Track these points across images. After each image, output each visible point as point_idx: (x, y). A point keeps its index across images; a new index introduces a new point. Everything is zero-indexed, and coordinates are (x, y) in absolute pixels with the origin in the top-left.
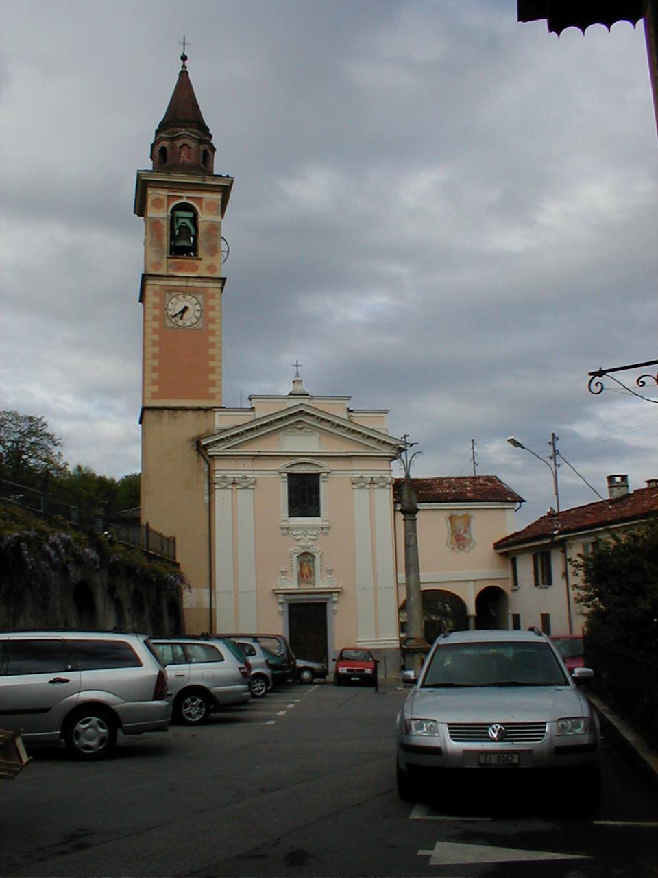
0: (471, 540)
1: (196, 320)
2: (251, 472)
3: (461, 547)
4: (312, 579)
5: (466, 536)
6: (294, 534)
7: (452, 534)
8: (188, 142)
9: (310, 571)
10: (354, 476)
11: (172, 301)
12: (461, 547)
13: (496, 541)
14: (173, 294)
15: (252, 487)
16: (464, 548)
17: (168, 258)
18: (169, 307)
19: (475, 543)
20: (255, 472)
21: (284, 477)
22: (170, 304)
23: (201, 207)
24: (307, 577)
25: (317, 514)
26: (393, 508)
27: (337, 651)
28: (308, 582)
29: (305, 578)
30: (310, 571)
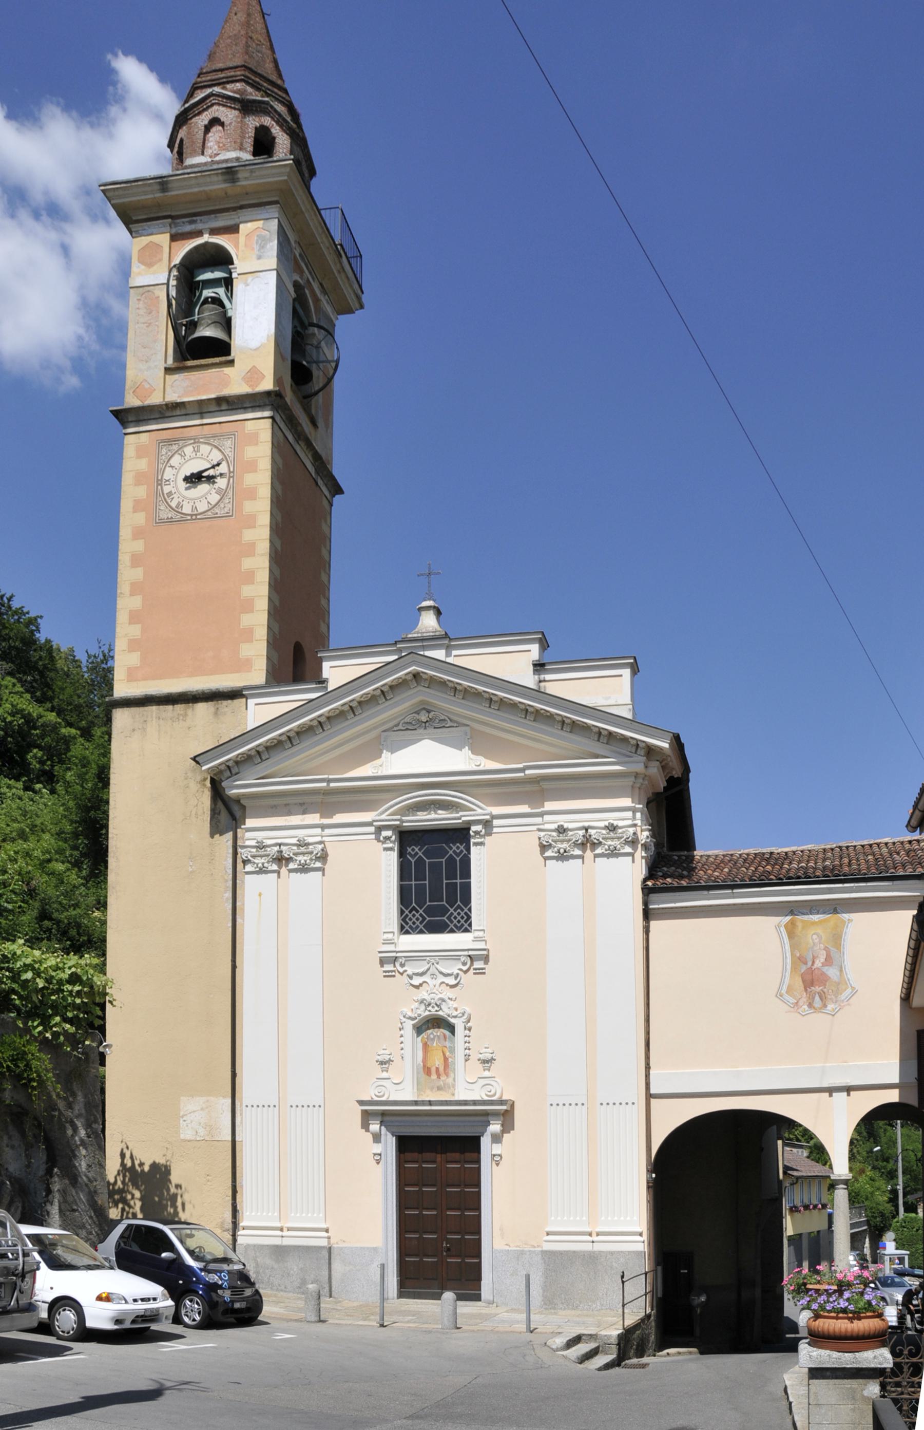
0: (842, 983)
1: (218, 497)
2: (318, 831)
3: (817, 1002)
4: (450, 1080)
5: (832, 972)
6: (410, 972)
7: (794, 968)
8: (219, 111)
9: (446, 1059)
10: (547, 826)
11: (172, 462)
12: (817, 1002)
13: (458, 751)
14: (175, 447)
15: (318, 864)
16: (825, 1006)
17: (168, 370)
18: (166, 477)
19: (854, 992)
20: (327, 831)
21: (387, 838)
22: (168, 469)
23: (237, 246)
24: (439, 1076)
25: (465, 926)
26: (640, 907)
27: (798, 1318)
28: (439, 1088)
29: (434, 1076)
30: (446, 1059)
